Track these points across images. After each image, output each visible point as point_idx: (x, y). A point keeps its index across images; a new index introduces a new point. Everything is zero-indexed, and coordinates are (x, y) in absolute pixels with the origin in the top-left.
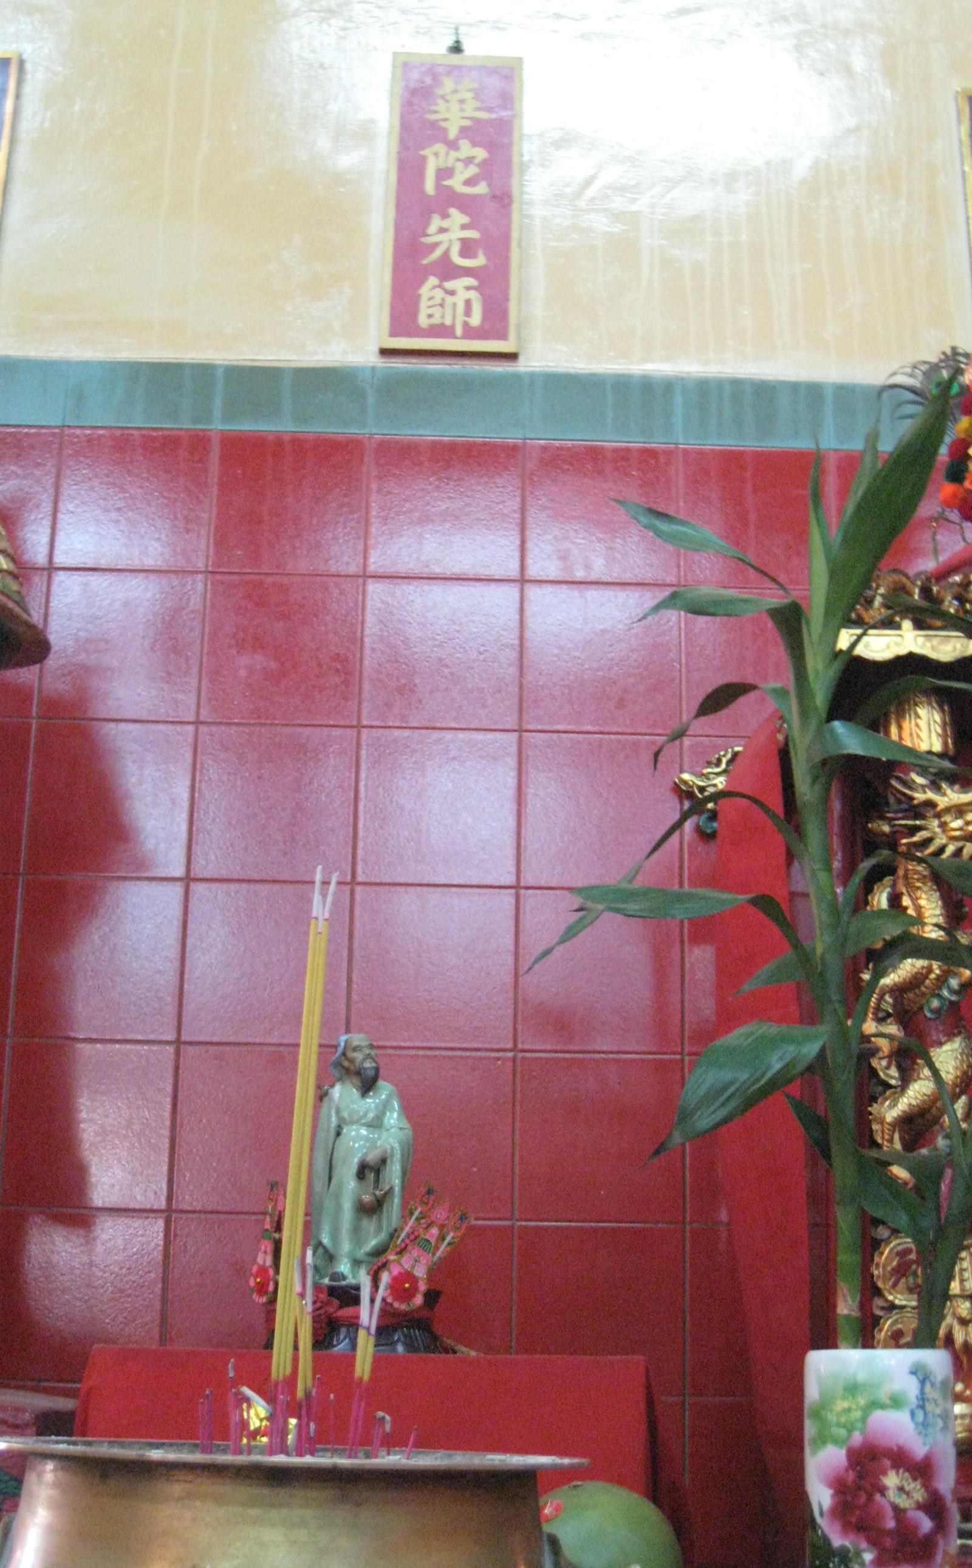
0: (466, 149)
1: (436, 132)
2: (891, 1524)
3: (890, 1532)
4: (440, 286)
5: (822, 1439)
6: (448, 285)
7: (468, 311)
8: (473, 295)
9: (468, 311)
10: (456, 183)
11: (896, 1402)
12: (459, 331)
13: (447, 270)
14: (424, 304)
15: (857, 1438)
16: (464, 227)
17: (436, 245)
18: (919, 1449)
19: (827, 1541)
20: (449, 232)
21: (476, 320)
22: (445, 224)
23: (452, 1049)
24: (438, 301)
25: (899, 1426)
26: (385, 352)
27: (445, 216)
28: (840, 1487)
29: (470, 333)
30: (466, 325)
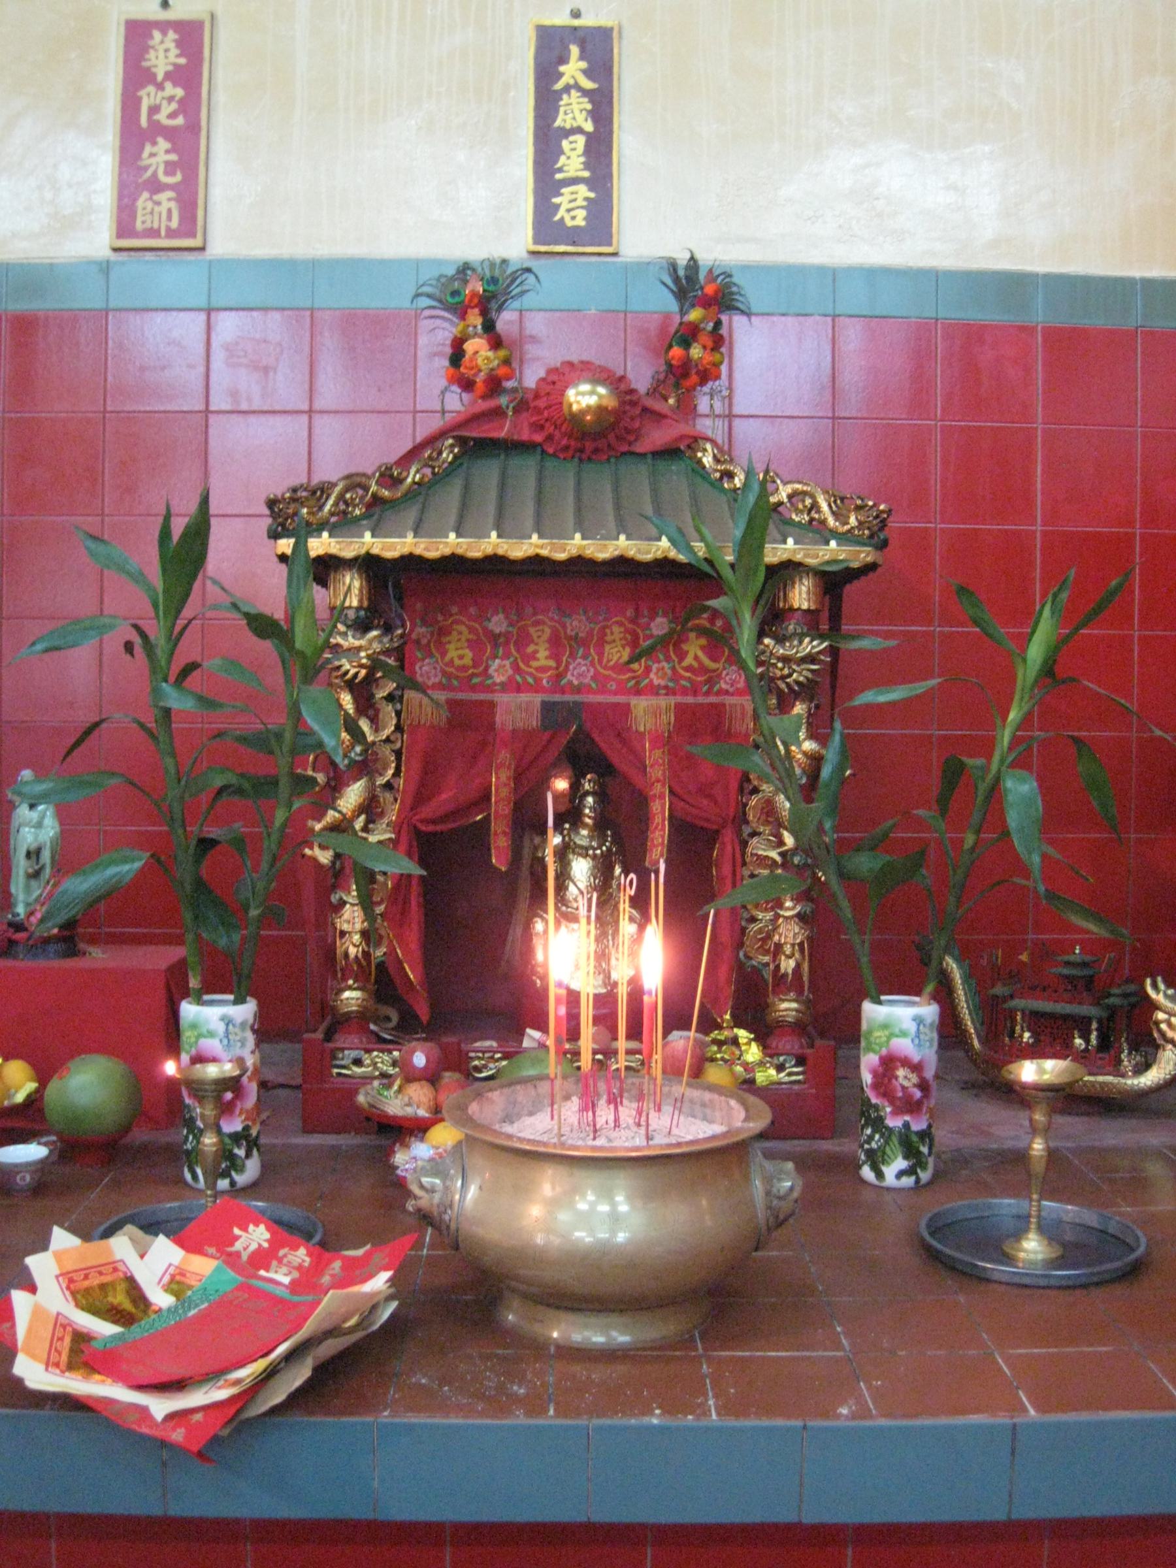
0: (170, 89)
2: (900, 1094)
3: (900, 1099)
4: (151, 199)
5: (869, 1049)
6: (155, 197)
7: (169, 218)
8: (173, 205)
9: (169, 218)
10: (162, 117)
11: (903, 1034)
12: (163, 233)
13: (155, 187)
14: (140, 213)
15: (884, 1051)
16: (167, 152)
17: (146, 168)
18: (916, 1058)
19: (869, 1100)
20: (158, 155)
21: (174, 224)
22: (155, 150)
24: (149, 209)
25: (905, 1046)
26: (115, 250)
27: (154, 143)
28: (875, 1074)
29: (171, 234)
30: (168, 229)
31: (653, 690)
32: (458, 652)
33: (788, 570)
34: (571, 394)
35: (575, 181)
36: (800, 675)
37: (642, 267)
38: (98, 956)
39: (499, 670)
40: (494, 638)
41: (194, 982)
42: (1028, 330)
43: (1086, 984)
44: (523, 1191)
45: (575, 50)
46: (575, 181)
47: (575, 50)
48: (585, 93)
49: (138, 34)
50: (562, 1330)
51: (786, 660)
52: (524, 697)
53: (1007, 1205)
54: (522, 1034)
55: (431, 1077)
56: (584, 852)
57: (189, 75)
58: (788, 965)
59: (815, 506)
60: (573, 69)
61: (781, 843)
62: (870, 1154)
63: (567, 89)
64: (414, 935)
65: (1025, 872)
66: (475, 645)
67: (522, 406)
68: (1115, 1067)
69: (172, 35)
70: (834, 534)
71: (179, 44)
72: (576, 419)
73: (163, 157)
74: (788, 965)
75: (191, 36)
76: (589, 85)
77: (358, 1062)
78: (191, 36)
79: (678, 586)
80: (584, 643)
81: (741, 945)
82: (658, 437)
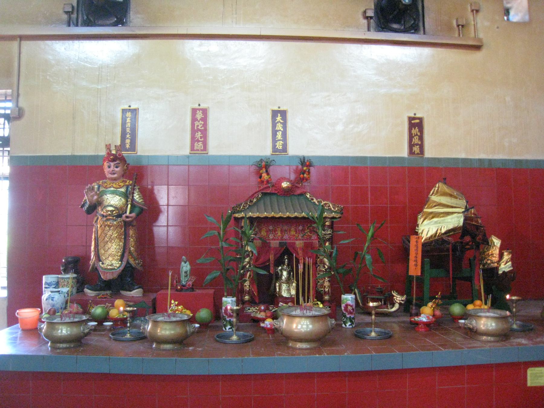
0: (201, 122)
1: (196, 120)
10: (199, 127)
20: (199, 135)
21: (202, 148)
23: (309, 269)
25: (349, 302)
29: (201, 150)
31: (300, 240)
32: (264, 233)
33: (325, 218)
34: (283, 184)
35: (280, 140)
36: (328, 237)
37: (293, 157)
38: (198, 291)
39: (271, 236)
40: (270, 230)
41: (225, 294)
42: (367, 167)
43: (381, 292)
44: (292, 323)
45: (279, 115)
46: (280, 140)
47: (279, 115)
48: (281, 123)
49: (194, 111)
50: (299, 345)
51: (325, 234)
52: (276, 241)
53: (369, 329)
54: (278, 304)
55: (264, 311)
56: (285, 270)
57: (205, 119)
58: (327, 290)
59: (329, 206)
60: (279, 118)
61: (325, 267)
62: (344, 322)
63: (278, 122)
64: (256, 287)
65: (369, 271)
66: (267, 232)
67: (273, 186)
68: (387, 308)
69: (201, 111)
70: (333, 211)
71: (202, 113)
72: (283, 188)
73: (200, 135)
74: (327, 290)
75: (205, 111)
76: (282, 121)
77: (249, 309)
78: (205, 111)
79: (306, 222)
80: (286, 231)
81: (316, 287)
82: (299, 192)
